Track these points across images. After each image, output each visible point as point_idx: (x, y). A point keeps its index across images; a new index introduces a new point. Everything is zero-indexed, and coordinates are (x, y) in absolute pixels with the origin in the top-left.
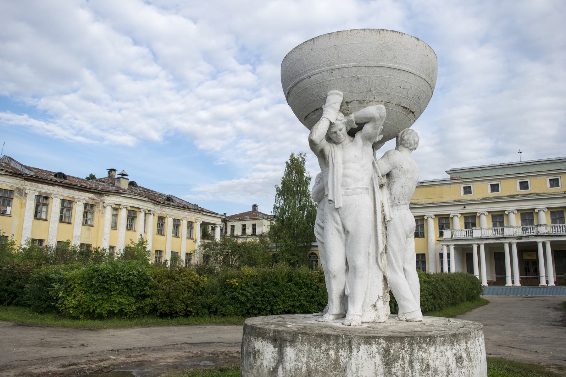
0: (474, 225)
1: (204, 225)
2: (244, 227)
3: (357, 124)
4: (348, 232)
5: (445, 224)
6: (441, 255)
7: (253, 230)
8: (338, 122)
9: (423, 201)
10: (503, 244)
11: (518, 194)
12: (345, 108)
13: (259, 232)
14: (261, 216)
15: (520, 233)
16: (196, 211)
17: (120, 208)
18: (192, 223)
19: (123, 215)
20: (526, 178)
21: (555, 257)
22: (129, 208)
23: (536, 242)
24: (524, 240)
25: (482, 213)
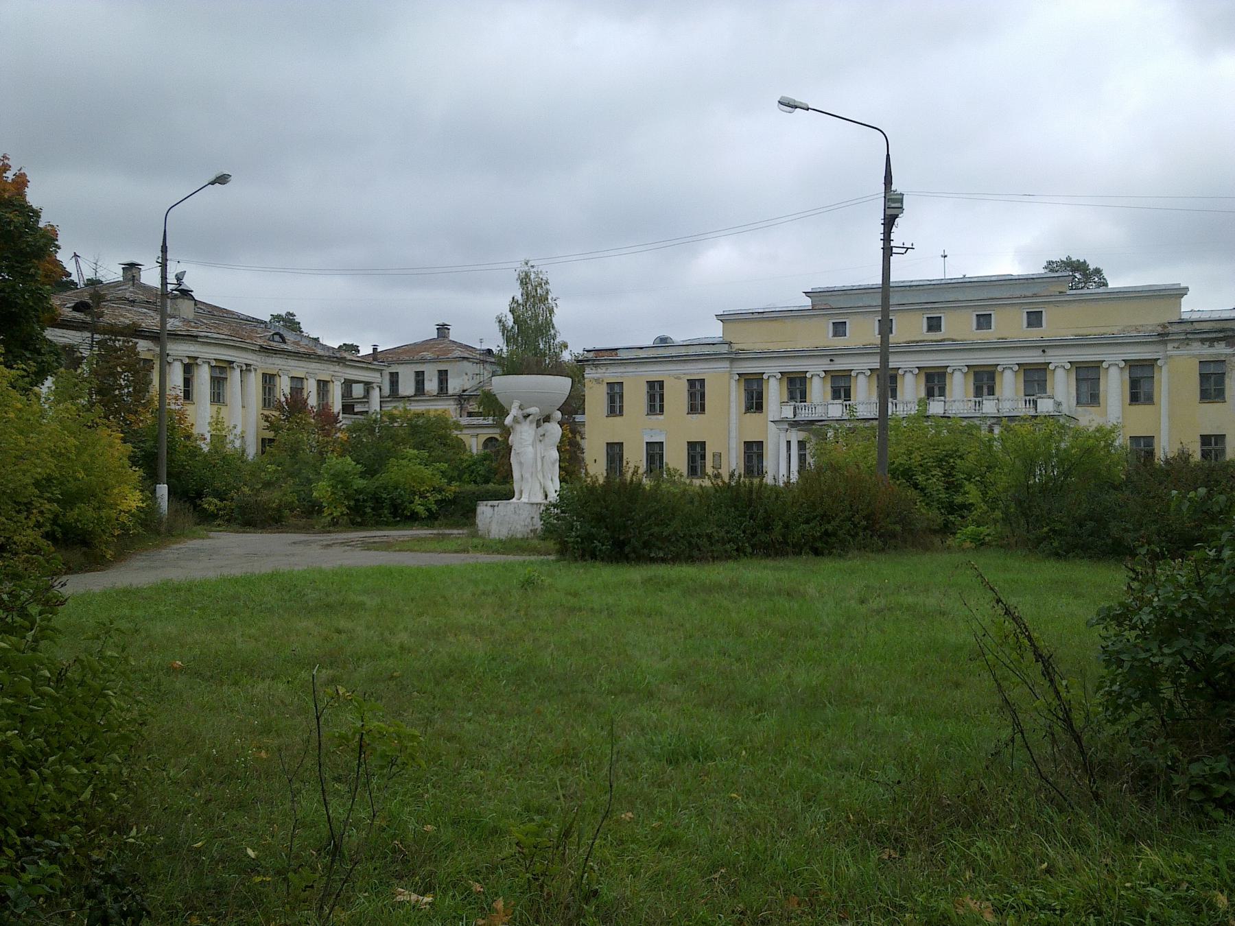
2: (420, 378)
6: (789, 443)
9: (758, 347)
12: (521, 408)
13: (455, 389)
14: (457, 353)
17: (197, 364)
18: (326, 383)
19: (203, 376)
22: (214, 363)
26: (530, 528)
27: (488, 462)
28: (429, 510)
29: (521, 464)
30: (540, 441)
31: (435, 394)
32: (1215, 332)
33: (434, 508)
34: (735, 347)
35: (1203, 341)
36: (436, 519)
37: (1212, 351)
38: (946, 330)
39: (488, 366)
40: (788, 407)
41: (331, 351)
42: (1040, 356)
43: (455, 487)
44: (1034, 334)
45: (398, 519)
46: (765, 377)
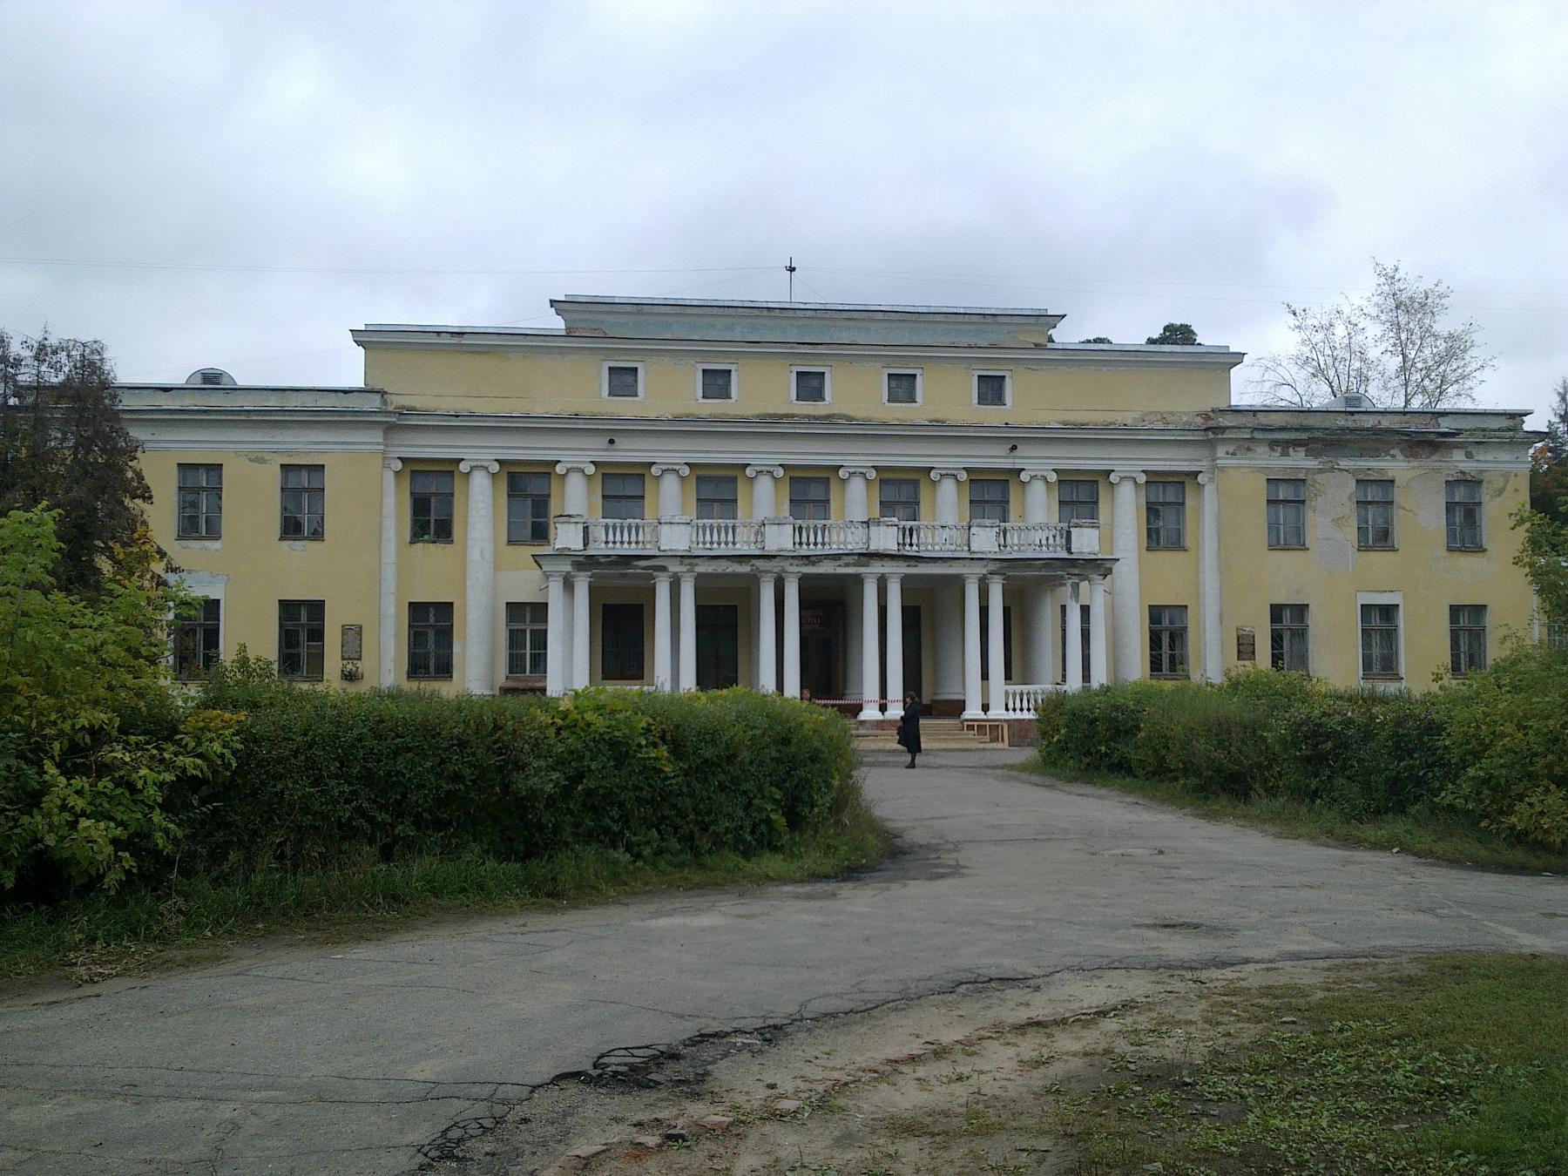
5: (435, 494)
10: (858, 580)
11: (790, 412)
20: (818, 363)
24: (923, 569)
25: (479, 464)
32: (1296, 430)
34: (396, 401)
35: (1273, 444)
37: (1287, 462)
38: (835, 399)
40: (572, 527)
42: (1005, 457)
44: (992, 415)
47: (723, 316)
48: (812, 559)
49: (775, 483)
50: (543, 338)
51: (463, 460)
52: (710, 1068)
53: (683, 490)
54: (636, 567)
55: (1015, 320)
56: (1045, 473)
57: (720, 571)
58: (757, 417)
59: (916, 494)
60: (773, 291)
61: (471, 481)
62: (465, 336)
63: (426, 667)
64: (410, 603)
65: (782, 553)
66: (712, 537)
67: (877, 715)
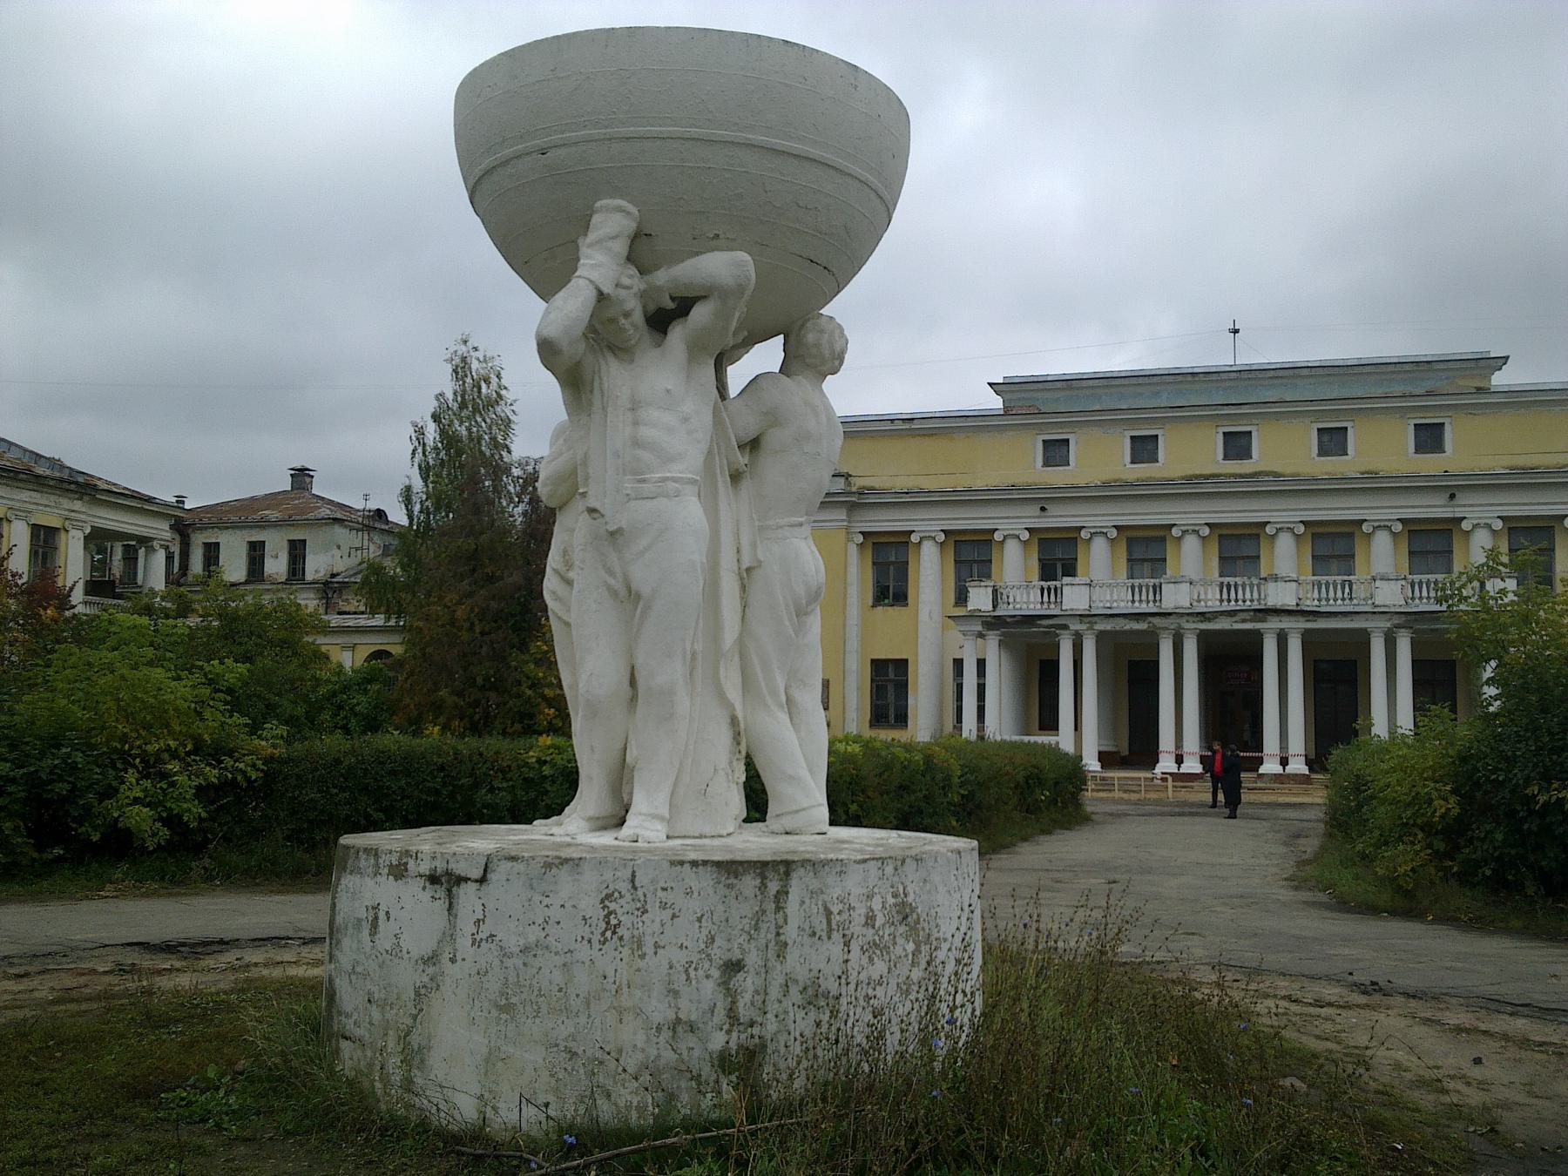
0: (1070, 570)
1: (98, 540)
2: (256, 553)
3: (673, 299)
4: (638, 596)
6: (958, 663)
7: (294, 563)
8: (623, 293)
9: (902, 483)
14: (325, 512)
15: (1212, 599)
16: (66, 486)
18: (52, 532)
20: (1245, 422)
21: (1316, 681)
23: (1365, 629)
24: (1321, 624)
26: (718, 1041)
27: (376, 687)
28: (172, 821)
29: (630, 599)
30: (736, 477)
31: (284, 580)
33: (193, 811)
34: (858, 483)
36: (198, 849)
39: (376, 538)
40: (982, 590)
41: (67, 471)
42: (1445, 506)
43: (270, 742)
44: (1430, 464)
45: (58, 851)
46: (914, 538)
47: (1341, 375)
48: (1207, 616)
49: (1394, 541)
50: (980, 418)
51: (1465, 518)
52: (707, 1071)
53: (1204, 552)
54: (1040, 626)
55: (1450, 365)
56: (1489, 521)
57: (1118, 628)
58: (1183, 478)
59: (1450, 544)
60: (1219, 356)
61: (1182, 545)
62: (915, 421)
63: (887, 717)
64: (872, 660)
65: (1177, 611)
66: (1244, 594)
67: (1278, 769)
